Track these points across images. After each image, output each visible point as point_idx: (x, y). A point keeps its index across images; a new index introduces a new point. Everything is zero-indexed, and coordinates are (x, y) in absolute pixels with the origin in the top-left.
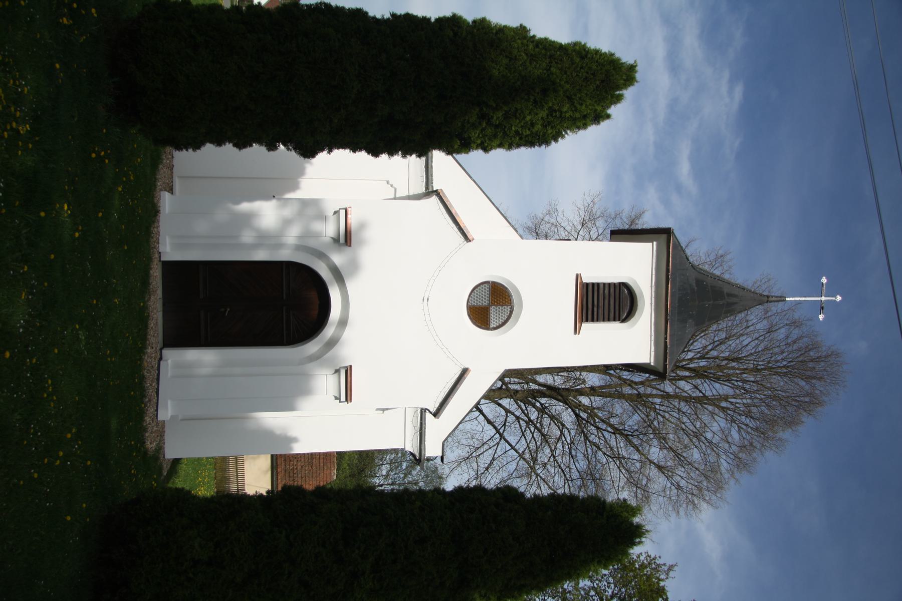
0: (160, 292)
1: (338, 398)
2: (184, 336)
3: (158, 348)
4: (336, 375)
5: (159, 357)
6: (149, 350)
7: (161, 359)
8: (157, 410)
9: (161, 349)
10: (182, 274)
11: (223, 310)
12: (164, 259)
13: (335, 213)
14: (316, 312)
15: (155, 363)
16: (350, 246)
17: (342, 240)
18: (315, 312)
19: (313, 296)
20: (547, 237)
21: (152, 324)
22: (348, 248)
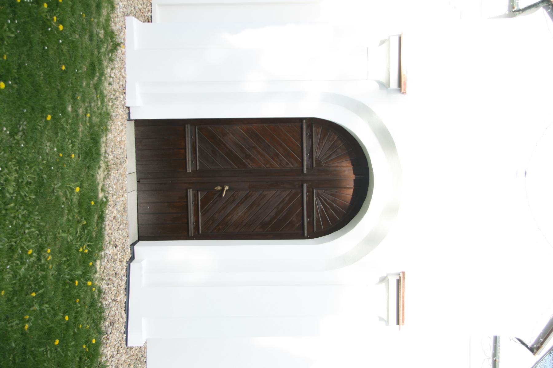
0: (130, 164)
1: (385, 86)
2: (166, 222)
3: (130, 241)
4: (383, 285)
5: (128, 256)
6: (109, 251)
7: (132, 258)
8: (126, 332)
9: (133, 245)
10: (161, 140)
11: (219, 188)
12: (137, 115)
13: (382, 42)
14: (351, 192)
15: (121, 269)
16: (404, 93)
17: (394, 83)
18: (349, 193)
19: (347, 170)
20: (124, 89)
21: (110, 213)
22: (399, 96)
